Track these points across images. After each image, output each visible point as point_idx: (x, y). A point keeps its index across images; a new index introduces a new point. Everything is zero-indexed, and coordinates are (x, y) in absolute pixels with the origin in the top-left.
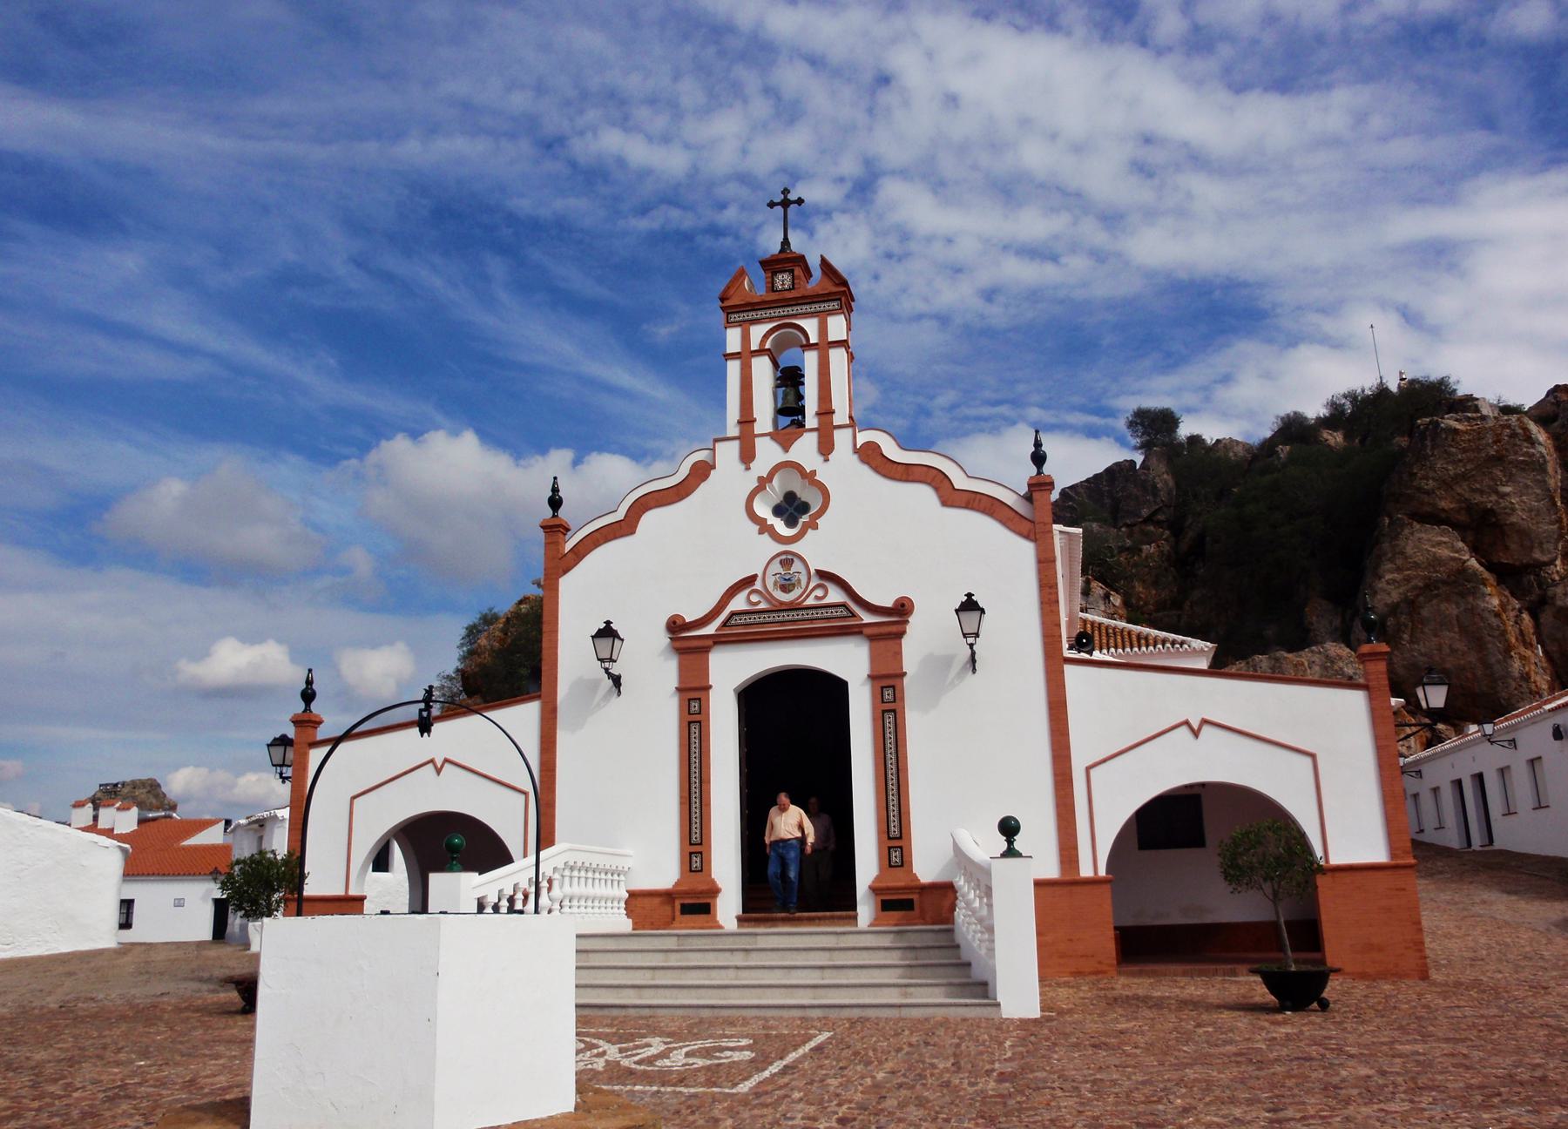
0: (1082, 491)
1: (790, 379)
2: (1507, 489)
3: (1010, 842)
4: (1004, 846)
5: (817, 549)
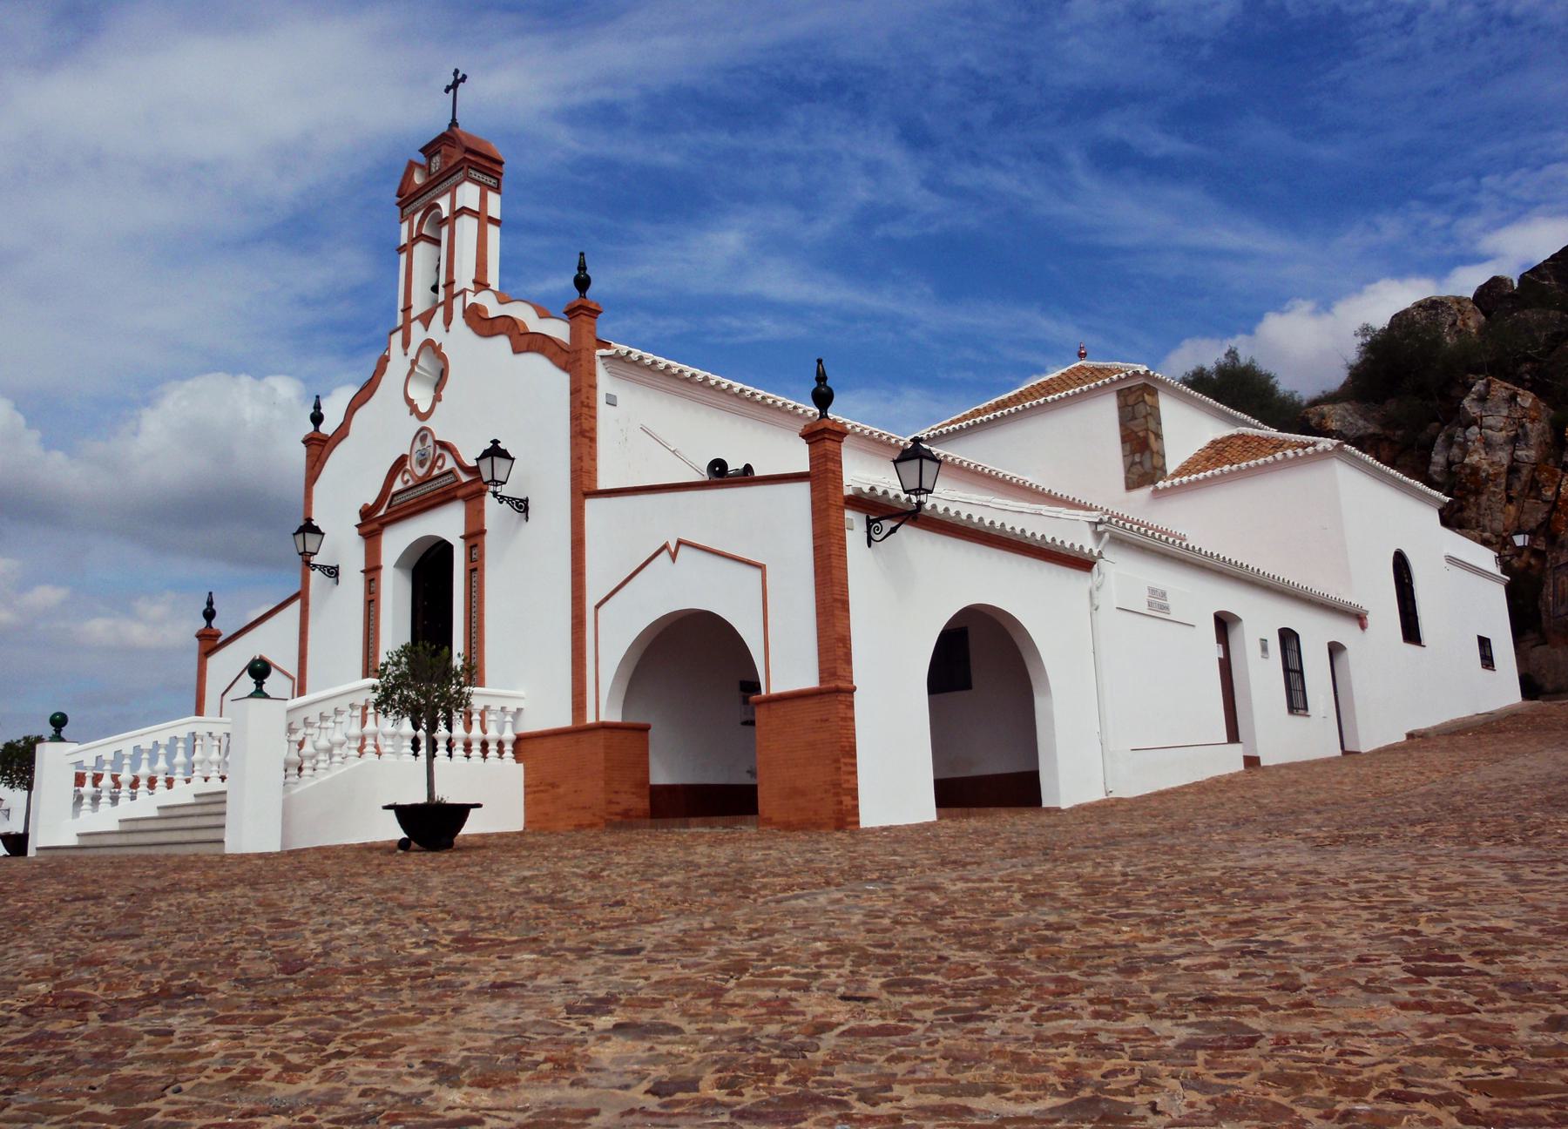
0: (1545, 271)
3: (259, 684)
4: (253, 688)
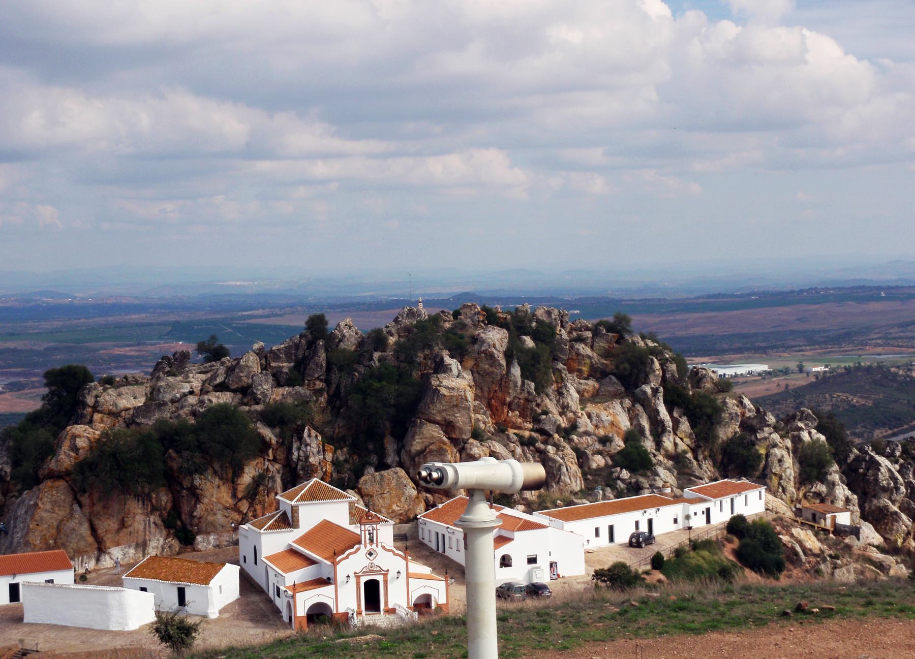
2: (458, 415)
5: (376, 562)
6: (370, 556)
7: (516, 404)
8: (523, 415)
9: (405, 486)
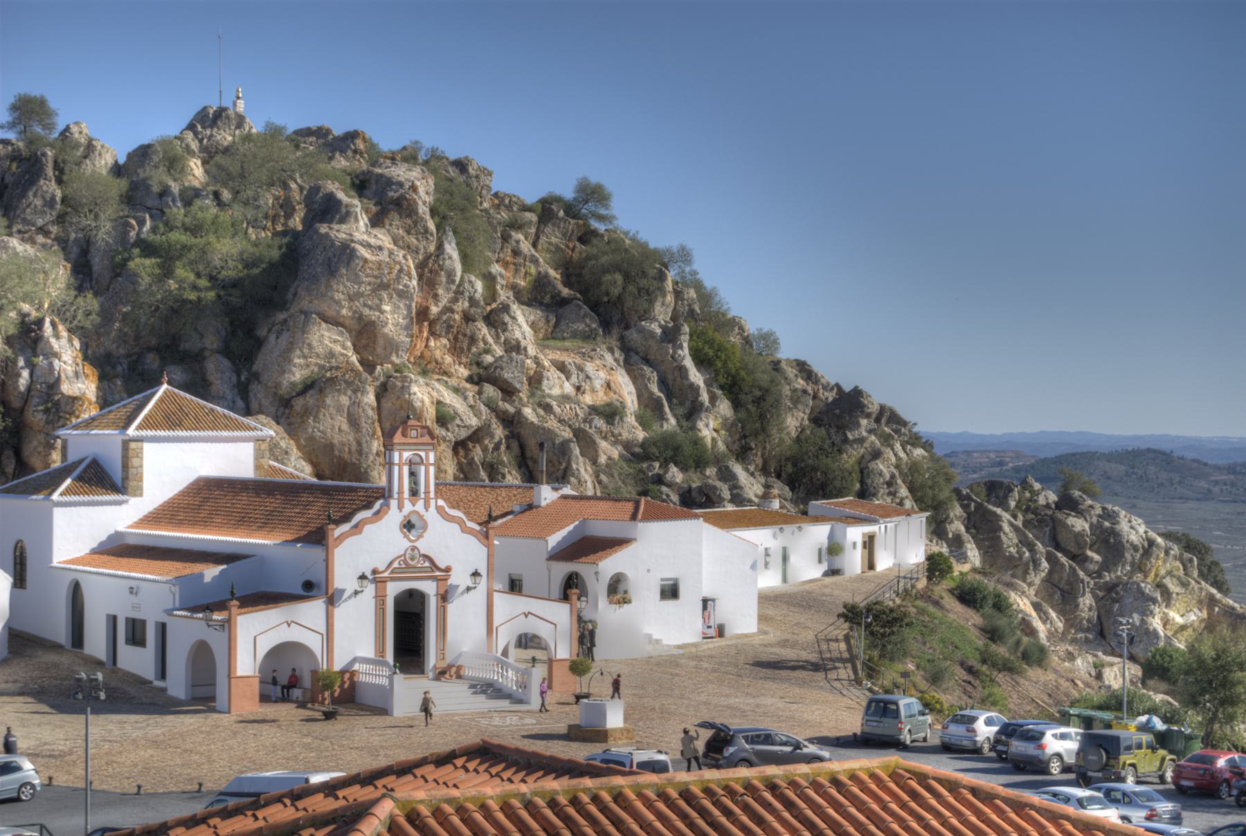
1: (412, 474)
5: (424, 546)
6: (409, 531)
7: (445, 322)
8: (455, 350)
9: (286, 453)
